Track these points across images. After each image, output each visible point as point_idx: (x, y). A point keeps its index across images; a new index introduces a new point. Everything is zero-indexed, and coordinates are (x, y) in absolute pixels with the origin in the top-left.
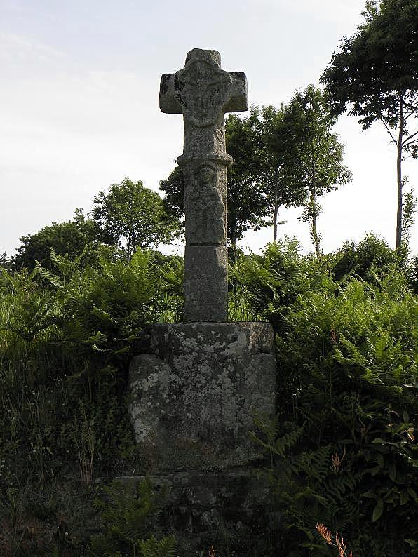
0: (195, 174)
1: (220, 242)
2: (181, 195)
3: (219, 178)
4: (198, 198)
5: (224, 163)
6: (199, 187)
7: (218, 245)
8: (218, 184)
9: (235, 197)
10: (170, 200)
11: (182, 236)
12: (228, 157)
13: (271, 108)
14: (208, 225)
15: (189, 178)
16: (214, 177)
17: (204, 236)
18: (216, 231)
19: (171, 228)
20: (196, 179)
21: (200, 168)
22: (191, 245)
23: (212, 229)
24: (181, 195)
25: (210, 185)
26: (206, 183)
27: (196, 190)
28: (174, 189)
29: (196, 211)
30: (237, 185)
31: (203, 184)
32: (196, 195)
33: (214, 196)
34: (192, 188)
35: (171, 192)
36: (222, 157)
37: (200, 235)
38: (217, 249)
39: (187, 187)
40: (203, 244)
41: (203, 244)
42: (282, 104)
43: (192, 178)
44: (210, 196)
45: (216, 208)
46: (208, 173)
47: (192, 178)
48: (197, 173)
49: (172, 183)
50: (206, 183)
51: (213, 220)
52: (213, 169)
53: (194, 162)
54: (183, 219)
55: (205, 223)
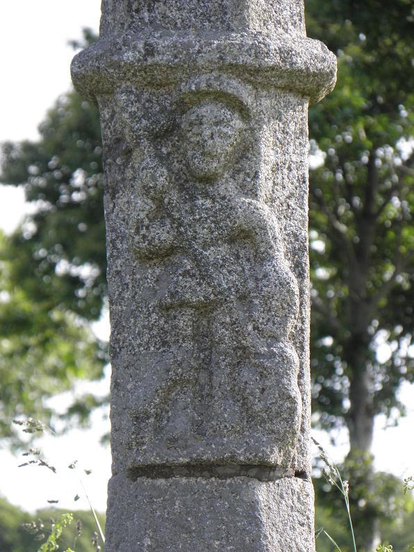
0: (157, 137)
1: (276, 457)
2: (93, 211)
3: (268, 153)
4: (172, 250)
5: (297, 83)
6: (174, 196)
7: (265, 471)
8: (265, 185)
9: (366, 218)
10: (51, 233)
11: (101, 421)
12: (312, 53)
13: (407, 140)
14: (221, 377)
15: (129, 152)
16: (246, 151)
17: (199, 429)
18: (258, 407)
19: (55, 372)
20: (162, 159)
21: (182, 107)
22: (138, 472)
23: (240, 397)
24: (93, 211)
25: (227, 187)
26: (209, 179)
27: (162, 211)
28: (67, 179)
29: (165, 309)
30: (372, 158)
31: (195, 182)
32: (163, 234)
33: (247, 239)
34: (141, 206)
35: (50, 194)
36: (286, 54)
37: (180, 424)
38: (263, 493)
39: (122, 200)
40: (198, 468)
41: (198, 468)
42: (407, 469)
43: (144, 157)
44: (231, 241)
45: (257, 293)
46: (217, 132)
47: (144, 157)
48: (168, 131)
49: (59, 149)
50: (209, 179)
51: (243, 355)
52: (242, 110)
53: (151, 78)
54: (102, 330)
55: (207, 365)
